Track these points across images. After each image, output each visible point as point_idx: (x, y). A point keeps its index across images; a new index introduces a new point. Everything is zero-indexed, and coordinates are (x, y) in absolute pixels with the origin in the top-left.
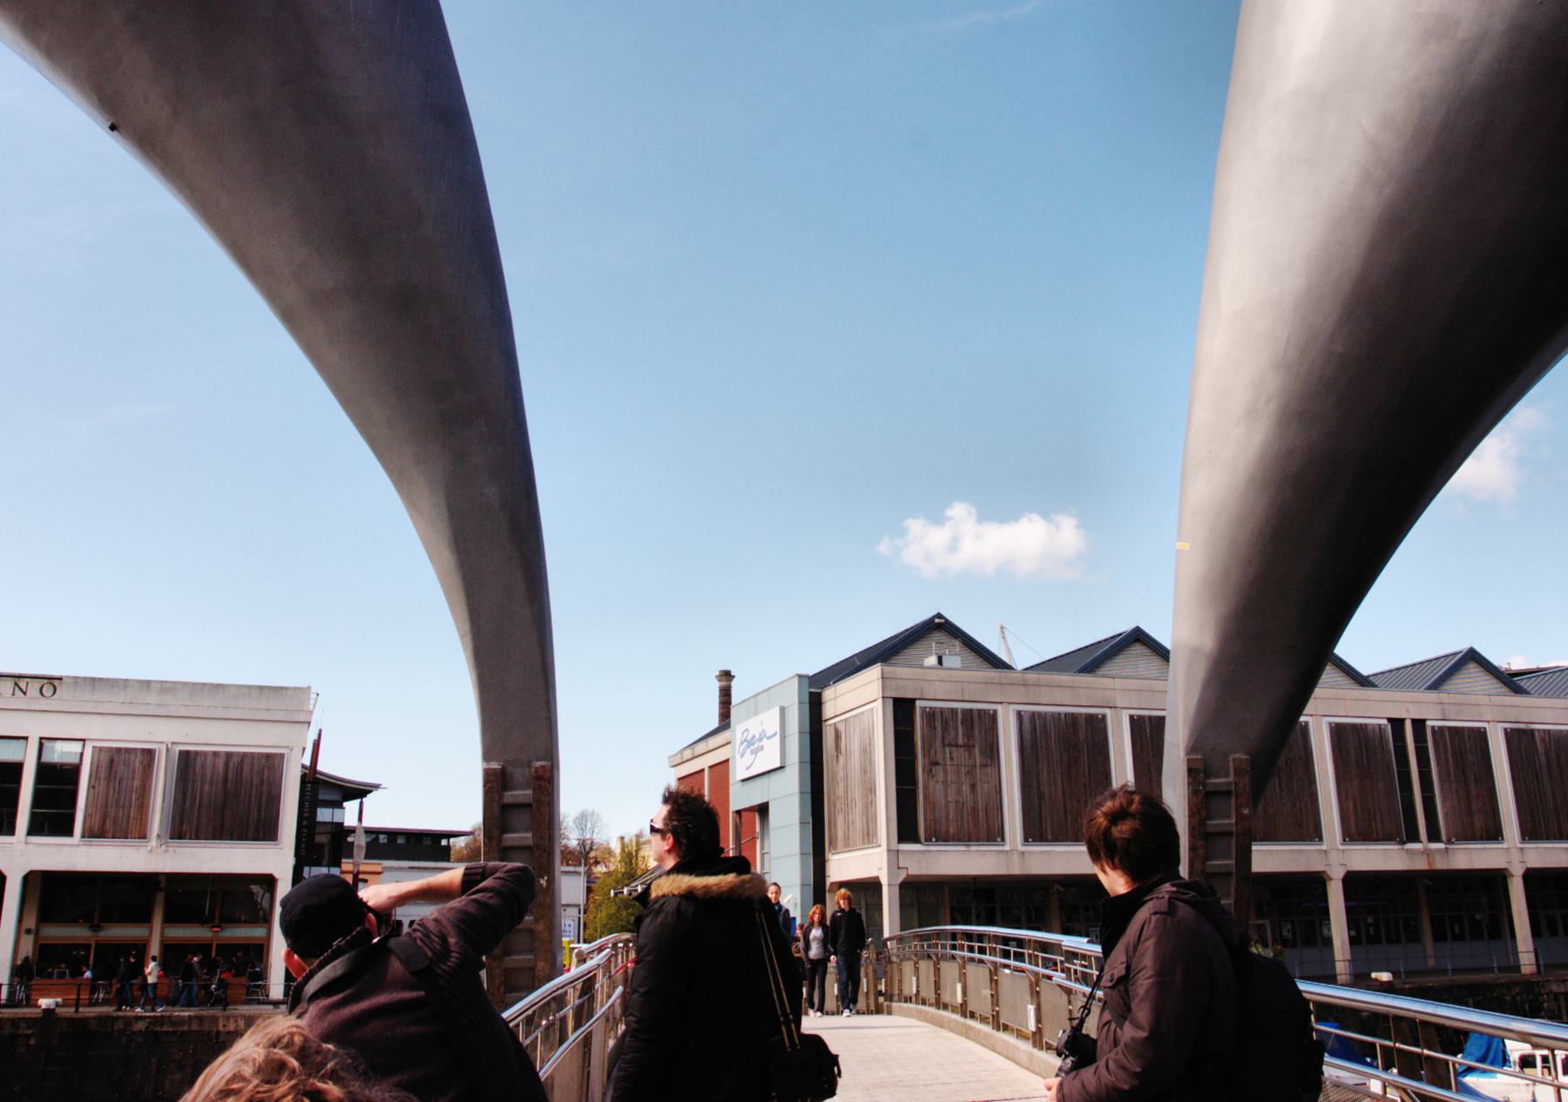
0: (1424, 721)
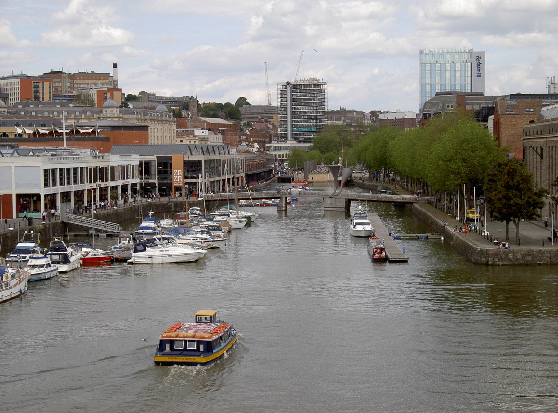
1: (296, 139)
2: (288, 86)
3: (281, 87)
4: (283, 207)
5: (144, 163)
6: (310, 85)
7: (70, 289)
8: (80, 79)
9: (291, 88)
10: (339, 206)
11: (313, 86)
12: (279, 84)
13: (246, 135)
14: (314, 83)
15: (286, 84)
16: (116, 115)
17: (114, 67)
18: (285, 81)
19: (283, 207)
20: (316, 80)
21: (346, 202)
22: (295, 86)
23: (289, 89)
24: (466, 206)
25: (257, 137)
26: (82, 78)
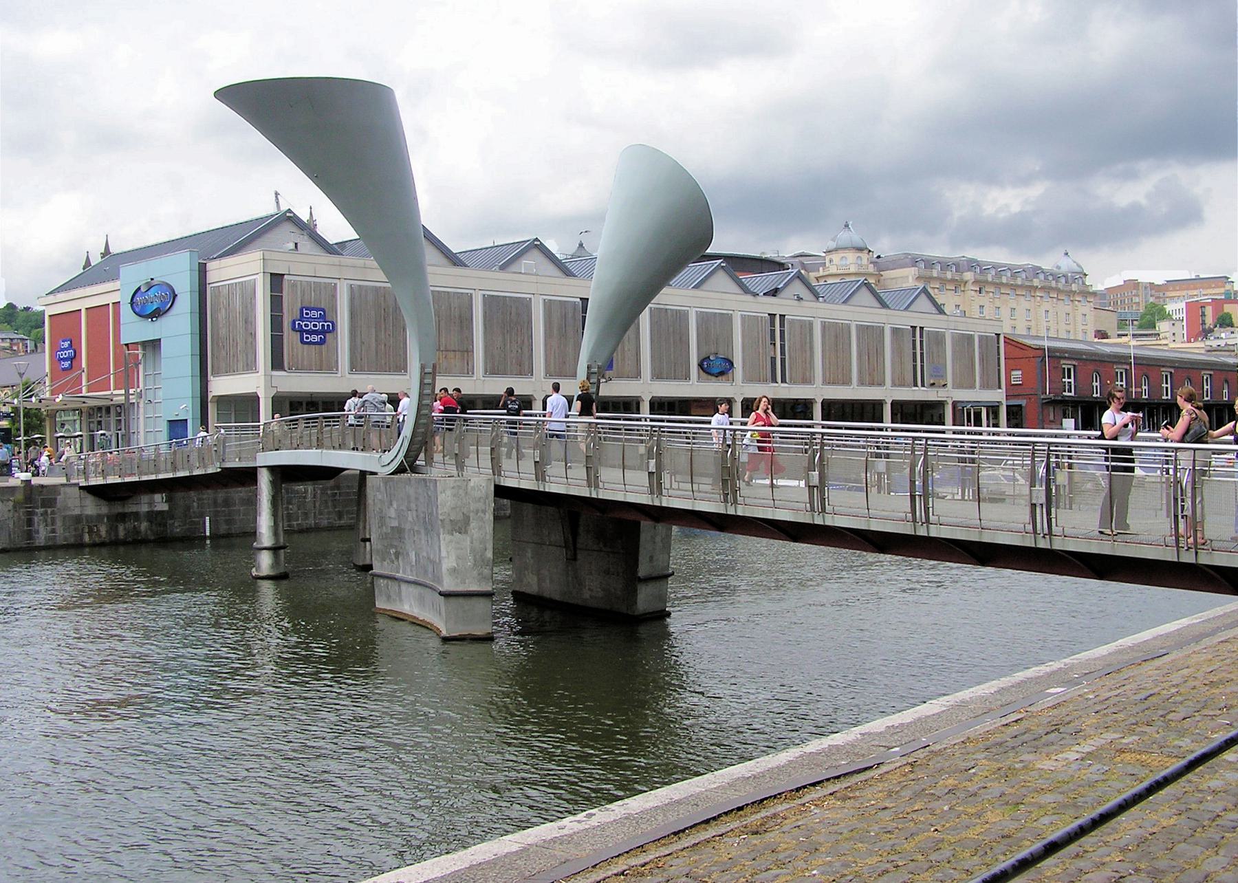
0: (784, 316)
8: (1175, 290)
16: (853, 269)
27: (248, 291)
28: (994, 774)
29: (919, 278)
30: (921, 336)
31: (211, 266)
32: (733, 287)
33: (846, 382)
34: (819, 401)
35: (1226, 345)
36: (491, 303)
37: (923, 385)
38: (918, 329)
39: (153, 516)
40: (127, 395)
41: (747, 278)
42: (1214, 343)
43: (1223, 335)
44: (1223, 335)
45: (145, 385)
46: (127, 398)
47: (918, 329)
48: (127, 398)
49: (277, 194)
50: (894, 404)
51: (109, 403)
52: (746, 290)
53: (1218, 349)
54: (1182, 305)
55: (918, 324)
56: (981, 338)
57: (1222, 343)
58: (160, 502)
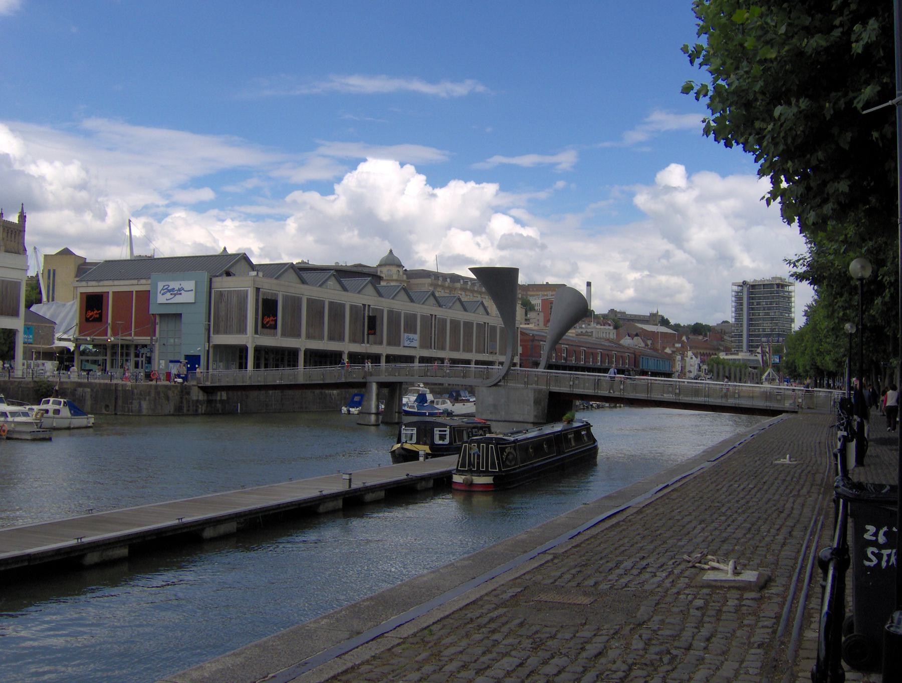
1: (751, 351)
2: (744, 286)
3: (736, 288)
4: (370, 414)
5: (137, 296)
6: (771, 285)
7: (590, 492)
8: (533, 291)
9: (748, 289)
10: (517, 418)
11: (775, 286)
12: (734, 284)
13: (682, 343)
14: (777, 282)
15: (742, 284)
16: (395, 277)
17: (587, 286)
18: (741, 281)
19: (370, 414)
20: (780, 279)
21: (537, 402)
22: (753, 286)
23: (745, 289)
24: (193, 516)
25: (706, 349)
26: (535, 289)
27: (243, 297)
28: (584, 556)
29: (431, 285)
30: (435, 320)
31: (214, 280)
32: (338, 286)
33: (341, 338)
34: (384, 355)
35: (586, 332)
36: (310, 302)
37: (435, 349)
38: (367, 306)
39: (221, 401)
40: (152, 339)
41: (346, 281)
42: (579, 331)
43: (583, 326)
44: (583, 326)
45: (160, 335)
46: (151, 342)
47: (367, 306)
48: (151, 342)
49: (23, 204)
50: (306, 351)
51: (130, 343)
52: (345, 289)
53: (582, 334)
54: (540, 301)
55: (367, 303)
56: (352, 307)
57: (584, 331)
58: (224, 395)
